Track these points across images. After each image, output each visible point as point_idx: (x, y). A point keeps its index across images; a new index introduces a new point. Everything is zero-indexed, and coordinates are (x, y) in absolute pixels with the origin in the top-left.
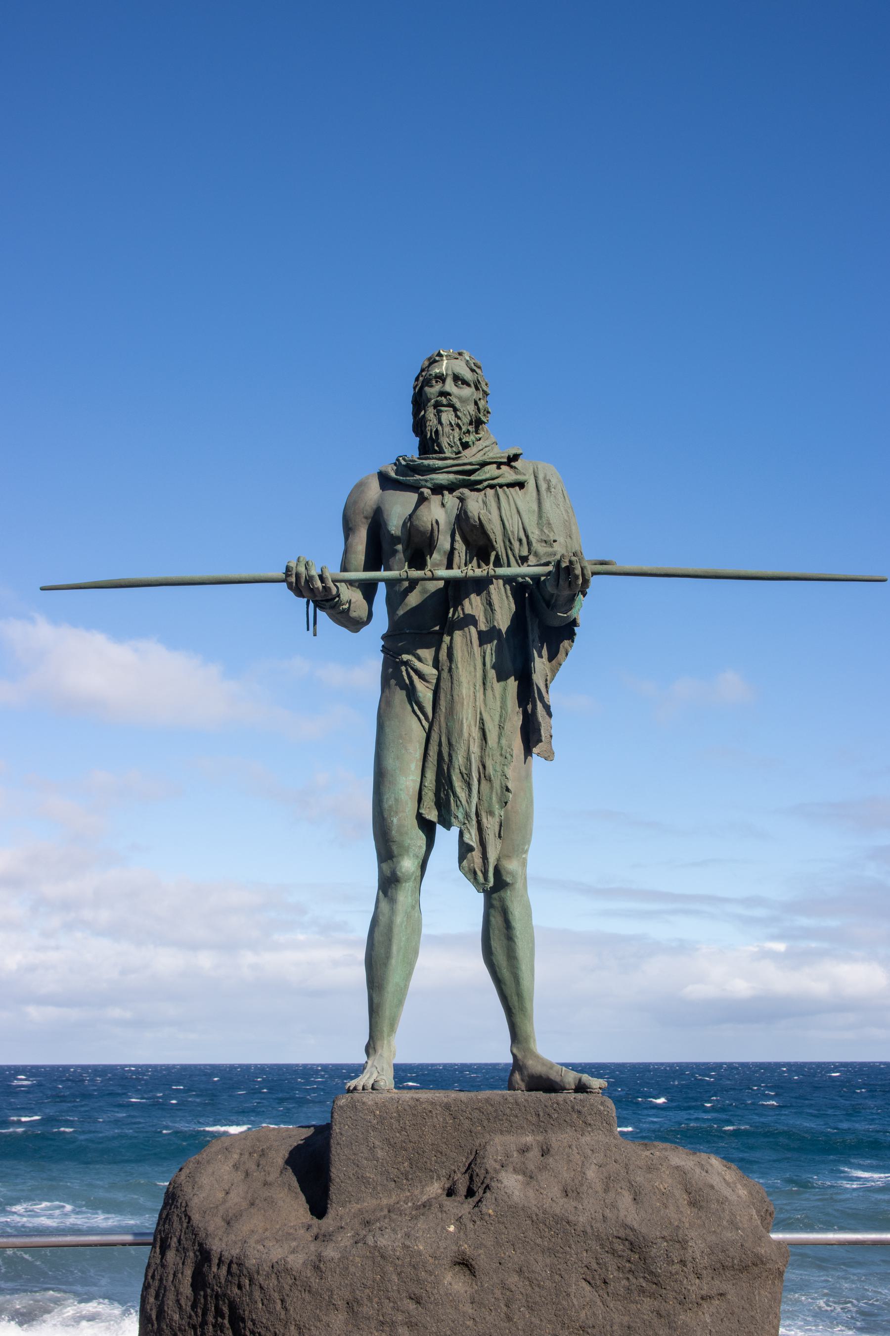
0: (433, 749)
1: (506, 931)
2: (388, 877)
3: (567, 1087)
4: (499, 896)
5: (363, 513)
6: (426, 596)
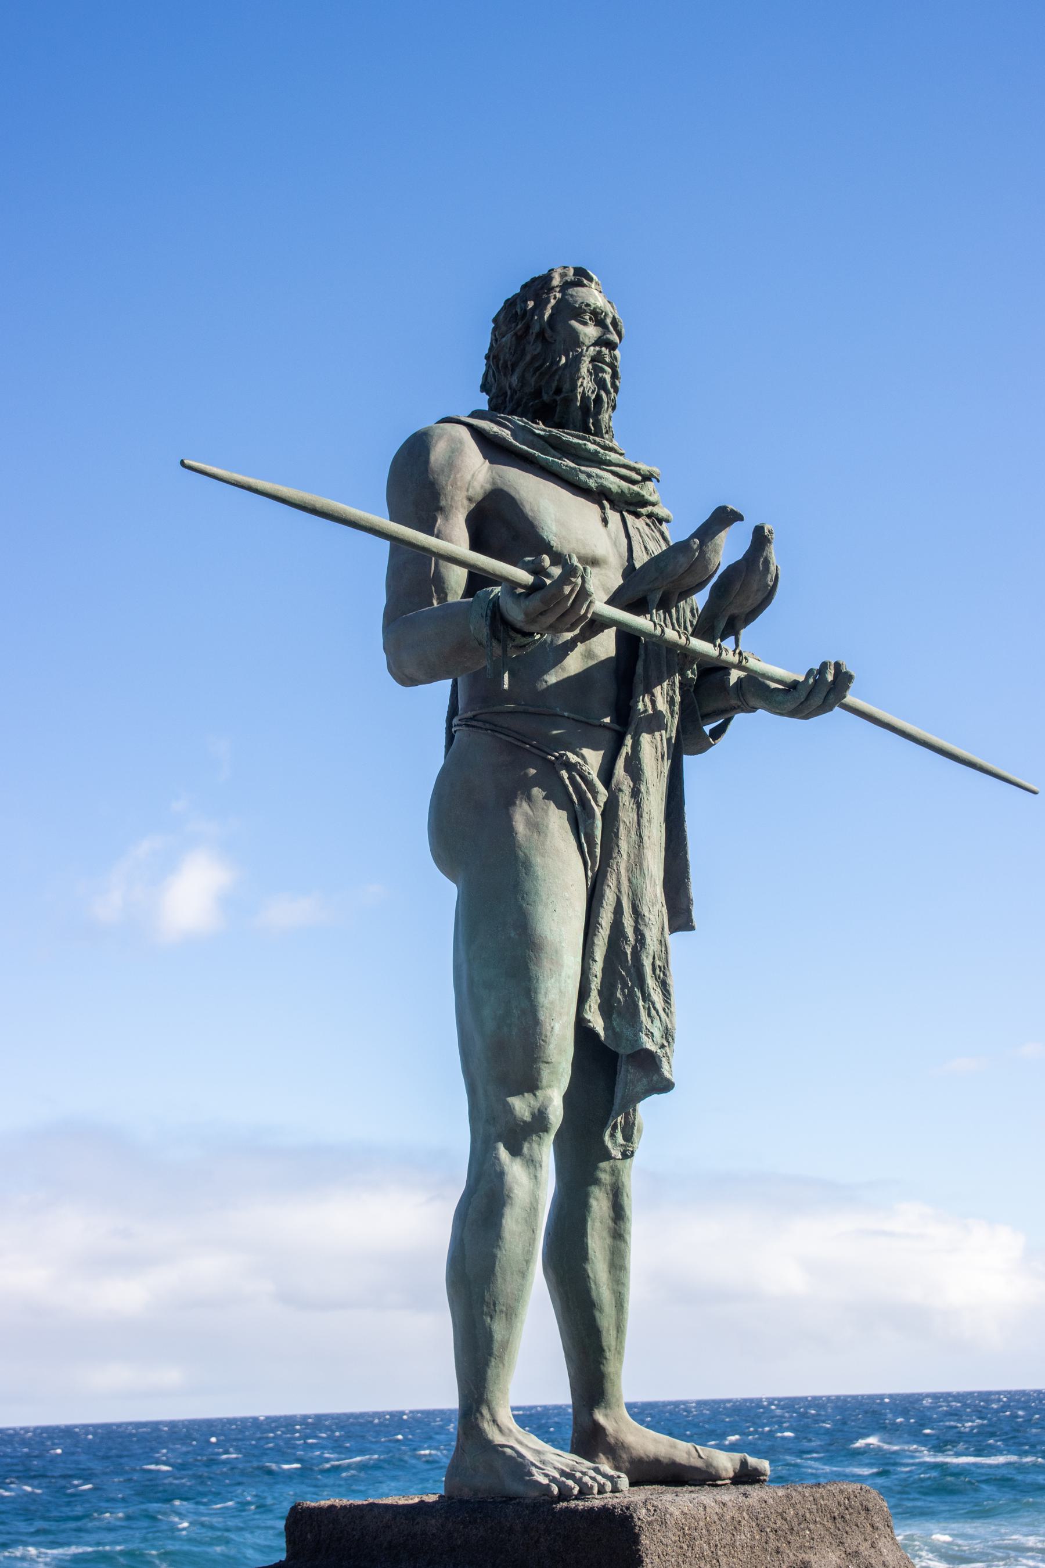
0: (607, 917)
1: (611, 1224)
2: (525, 1122)
3: (724, 1474)
4: (611, 1167)
5: (468, 490)
6: (591, 663)
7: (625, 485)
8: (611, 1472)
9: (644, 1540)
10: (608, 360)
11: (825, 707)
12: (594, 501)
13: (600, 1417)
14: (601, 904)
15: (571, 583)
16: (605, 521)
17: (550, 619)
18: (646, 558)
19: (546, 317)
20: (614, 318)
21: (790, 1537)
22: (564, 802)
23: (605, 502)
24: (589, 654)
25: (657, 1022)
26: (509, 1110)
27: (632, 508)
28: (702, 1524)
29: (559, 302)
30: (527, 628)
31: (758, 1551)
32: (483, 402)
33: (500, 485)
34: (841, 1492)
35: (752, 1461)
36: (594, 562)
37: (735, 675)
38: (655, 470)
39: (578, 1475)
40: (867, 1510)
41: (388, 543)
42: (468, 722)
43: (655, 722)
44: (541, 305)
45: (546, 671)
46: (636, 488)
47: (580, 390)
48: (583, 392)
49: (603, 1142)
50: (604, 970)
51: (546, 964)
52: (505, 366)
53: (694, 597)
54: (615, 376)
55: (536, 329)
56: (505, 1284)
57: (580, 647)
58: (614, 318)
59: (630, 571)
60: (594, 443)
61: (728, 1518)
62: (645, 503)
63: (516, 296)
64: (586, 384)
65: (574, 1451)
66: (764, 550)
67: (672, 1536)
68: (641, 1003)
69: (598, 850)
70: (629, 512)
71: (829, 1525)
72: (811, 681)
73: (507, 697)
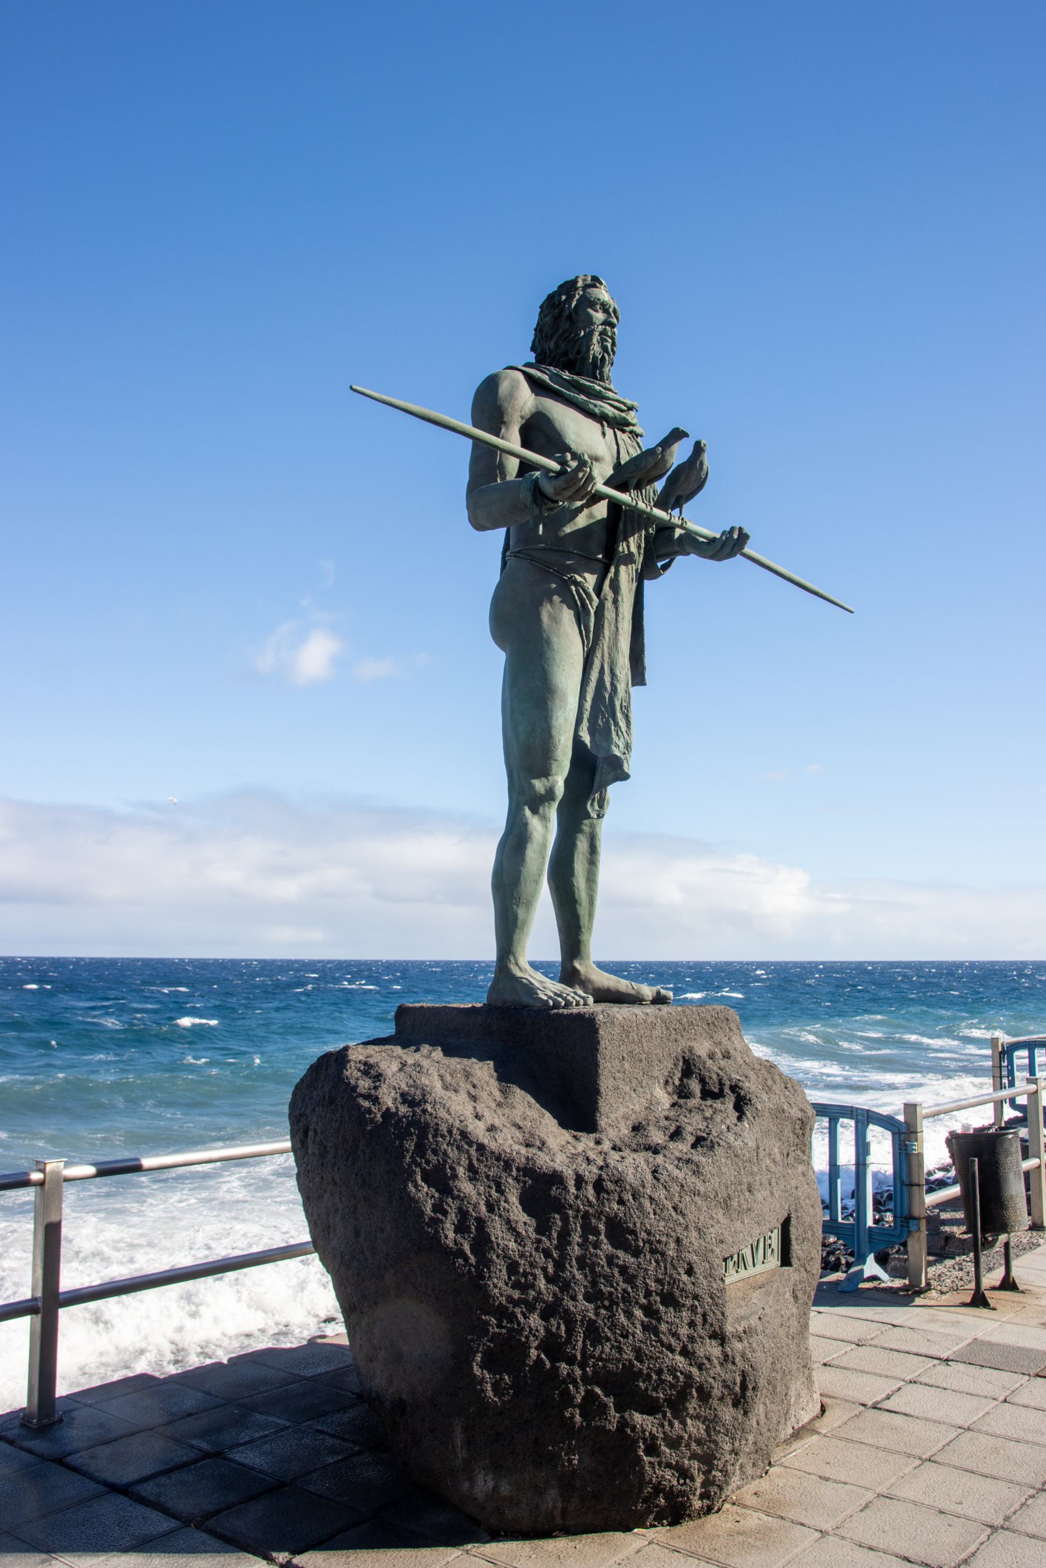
1: (589, 856)
3: (647, 998)
6: (592, 521)
7: (616, 412)
8: (583, 995)
9: (601, 1032)
10: (610, 334)
11: (731, 554)
12: (598, 422)
13: (577, 964)
14: (591, 668)
15: (583, 471)
16: (604, 434)
17: (569, 493)
18: (628, 458)
19: (573, 305)
20: (614, 309)
21: (683, 1033)
22: (572, 605)
23: (604, 423)
24: (591, 516)
25: (622, 739)
26: (532, 787)
27: (620, 427)
28: (634, 1024)
29: (581, 297)
30: (555, 498)
31: (665, 1040)
32: (531, 358)
33: (541, 410)
34: (714, 1010)
35: (663, 992)
36: (597, 459)
37: (678, 532)
38: (635, 404)
39: (564, 995)
40: (727, 1020)
41: (471, 441)
42: (516, 555)
43: (629, 559)
44: (570, 298)
45: (564, 525)
46: (623, 415)
47: (592, 352)
48: (594, 354)
49: (586, 808)
50: (592, 707)
51: (558, 702)
52: (546, 337)
53: (655, 483)
54: (613, 344)
55: (566, 313)
56: (526, 887)
57: (586, 511)
58: (614, 309)
59: (617, 466)
60: (599, 385)
61: (649, 1021)
62: (628, 424)
63: (555, 292)
64: (596, 349)
65: (561, 981)
66: (700, 456)
67: (617, 1030)
68: (613, 727)
69: (591, 635)
70: (619, 429)
71: (706, 1027)
72: (724, 538)
73: (540, 539)
